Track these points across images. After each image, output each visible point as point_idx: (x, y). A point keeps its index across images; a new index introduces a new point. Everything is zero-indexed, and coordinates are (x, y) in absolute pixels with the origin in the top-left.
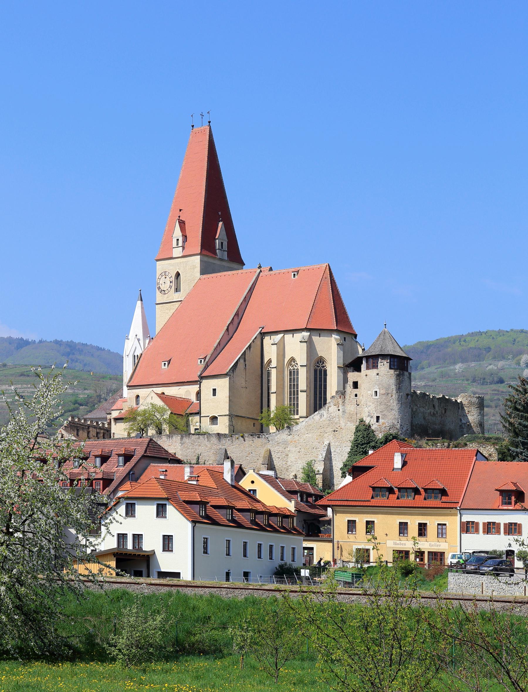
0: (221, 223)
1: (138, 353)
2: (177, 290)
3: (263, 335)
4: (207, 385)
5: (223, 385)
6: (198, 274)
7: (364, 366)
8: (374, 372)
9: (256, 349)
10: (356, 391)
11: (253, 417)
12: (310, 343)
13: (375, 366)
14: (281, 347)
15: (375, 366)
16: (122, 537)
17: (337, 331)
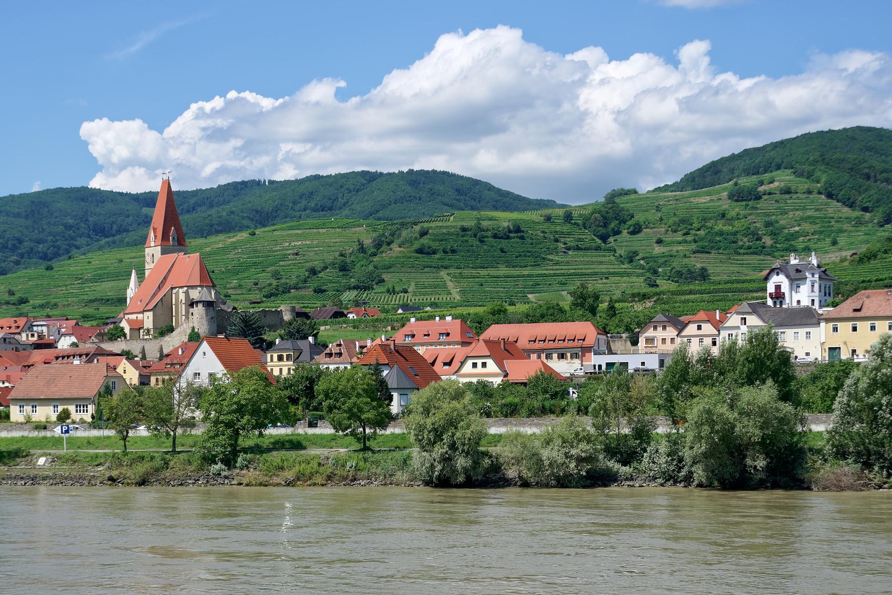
3: (172, 288)
5: (150, 314)
12: (187, 293)
14: (177, 294)
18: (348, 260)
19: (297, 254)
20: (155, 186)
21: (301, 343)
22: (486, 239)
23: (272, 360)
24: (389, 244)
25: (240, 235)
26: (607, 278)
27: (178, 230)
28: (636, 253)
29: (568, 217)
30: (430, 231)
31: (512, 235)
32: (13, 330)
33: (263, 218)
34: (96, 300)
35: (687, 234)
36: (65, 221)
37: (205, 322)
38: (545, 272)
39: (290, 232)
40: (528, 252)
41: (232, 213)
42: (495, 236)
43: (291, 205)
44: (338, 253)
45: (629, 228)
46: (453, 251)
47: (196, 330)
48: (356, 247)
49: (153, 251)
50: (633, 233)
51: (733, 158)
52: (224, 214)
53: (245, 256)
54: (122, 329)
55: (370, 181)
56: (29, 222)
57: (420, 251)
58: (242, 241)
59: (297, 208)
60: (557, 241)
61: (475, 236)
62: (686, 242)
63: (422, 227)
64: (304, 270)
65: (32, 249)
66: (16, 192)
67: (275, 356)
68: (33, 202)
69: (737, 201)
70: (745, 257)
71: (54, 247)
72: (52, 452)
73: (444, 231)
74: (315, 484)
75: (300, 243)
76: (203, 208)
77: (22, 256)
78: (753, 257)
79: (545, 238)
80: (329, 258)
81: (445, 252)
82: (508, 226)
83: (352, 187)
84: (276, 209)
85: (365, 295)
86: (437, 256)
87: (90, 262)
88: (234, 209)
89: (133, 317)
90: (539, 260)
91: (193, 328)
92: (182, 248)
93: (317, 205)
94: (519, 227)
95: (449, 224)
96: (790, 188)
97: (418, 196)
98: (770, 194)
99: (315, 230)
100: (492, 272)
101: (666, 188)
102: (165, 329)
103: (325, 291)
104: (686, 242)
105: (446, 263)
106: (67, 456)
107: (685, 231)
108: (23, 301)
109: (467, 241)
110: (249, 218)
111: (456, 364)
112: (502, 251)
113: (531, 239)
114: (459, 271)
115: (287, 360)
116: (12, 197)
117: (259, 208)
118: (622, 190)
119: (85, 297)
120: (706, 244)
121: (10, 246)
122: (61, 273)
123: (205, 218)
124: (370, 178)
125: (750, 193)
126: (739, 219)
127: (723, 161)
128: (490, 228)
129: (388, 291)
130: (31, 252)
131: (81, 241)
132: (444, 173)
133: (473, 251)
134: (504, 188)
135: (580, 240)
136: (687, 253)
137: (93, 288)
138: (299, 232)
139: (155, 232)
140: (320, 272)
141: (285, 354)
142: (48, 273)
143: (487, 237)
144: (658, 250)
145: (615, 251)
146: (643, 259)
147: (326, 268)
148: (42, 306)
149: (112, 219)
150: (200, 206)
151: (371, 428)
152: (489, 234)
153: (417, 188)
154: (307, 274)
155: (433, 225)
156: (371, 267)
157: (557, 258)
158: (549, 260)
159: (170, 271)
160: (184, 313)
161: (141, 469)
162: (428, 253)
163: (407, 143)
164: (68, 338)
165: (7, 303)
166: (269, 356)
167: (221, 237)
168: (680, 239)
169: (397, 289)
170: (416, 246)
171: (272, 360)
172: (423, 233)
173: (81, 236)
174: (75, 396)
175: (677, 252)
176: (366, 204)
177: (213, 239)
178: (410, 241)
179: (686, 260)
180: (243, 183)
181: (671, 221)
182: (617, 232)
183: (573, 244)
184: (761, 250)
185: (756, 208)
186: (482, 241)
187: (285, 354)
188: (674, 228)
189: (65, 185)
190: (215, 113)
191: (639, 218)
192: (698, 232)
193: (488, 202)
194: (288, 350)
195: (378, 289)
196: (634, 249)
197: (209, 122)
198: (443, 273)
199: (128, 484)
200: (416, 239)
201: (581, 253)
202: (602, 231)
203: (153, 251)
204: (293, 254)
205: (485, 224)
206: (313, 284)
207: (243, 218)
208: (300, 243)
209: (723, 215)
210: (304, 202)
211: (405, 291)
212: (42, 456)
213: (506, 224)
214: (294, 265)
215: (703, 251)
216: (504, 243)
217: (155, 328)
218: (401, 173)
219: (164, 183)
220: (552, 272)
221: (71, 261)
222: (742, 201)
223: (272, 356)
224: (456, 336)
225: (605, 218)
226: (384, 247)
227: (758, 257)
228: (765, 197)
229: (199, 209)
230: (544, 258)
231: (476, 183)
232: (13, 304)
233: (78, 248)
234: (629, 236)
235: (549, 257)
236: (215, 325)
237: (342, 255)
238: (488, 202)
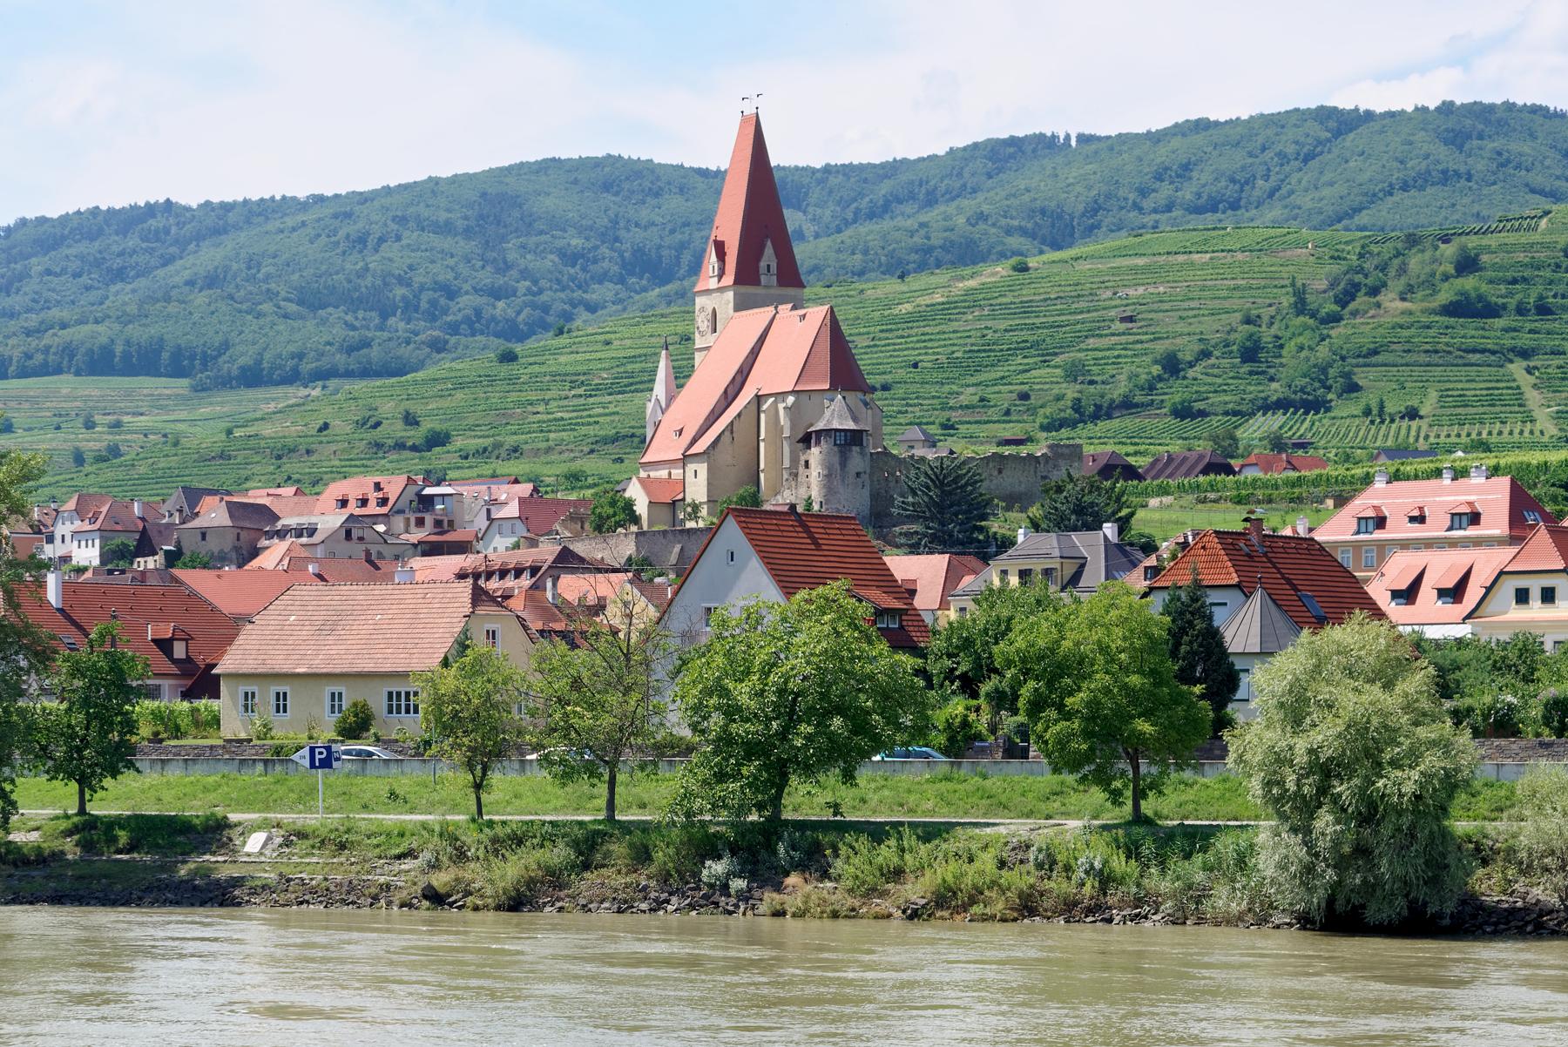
5: (702, 469)
18: (1267, 335)
19: (1130, 319)
21: (1082, 541)
24: (1374, 291)
32: (373, 508)
33: (1058, 230)
34: (615, 439)
36: (560, 243)
41: (982, 217)
44: (1238, 316)
48: (1287, 301)
52: (961, 220)
54: (629, 505)
55: (1338, 134)
56: (472, 246)
57: (1460, 309)
58: (994, 285)
59: (1147, 204)
63: (1463, 249)
64: (1148, 359)
65: (478, 312)
66: (445, 173)
68: (484, 195)
71: (534, 306)
72: (287, 817)
73: (1521, 257)
74: (985, 918)
76: (908, 208)
77: (454, 329)
80: (1211, 328)
83: (1291, 149)
84: (1095, 209)
85: (1307, 424)
86: (1499, 323)
87: (608, 343)
88: (985, 208)
92: (791, 291)
93: (1199, 195)
95: (1535, 237)
97: (1463, 169)
99: (1181, 258)
103: (1203, 414)
105: (1525, 340)
106: (323, 832)
108: (437, 440)
110: (1023, 232)
111: (1473, 594)
116: (434, 182)
119: (591, 430)
121: (424, 305)
122: (536, 369)
124: (1339, 124)
129: (1367, 412)
130: (475, 323)
131: (597, 293)
132: (1536, 110)
137: (612, 409)
140: (1191, 365)
142: (504, 370)
147: (1206, 354)
148: (483, 452)
149: (678, 237)
151: (1152, 762)
153: (1461, 148)
154: (1156, 370)
155: (1492, 241)
156: (1323, 352)
161: (512, 870)
165: (400, 446)
167: (941, 277)
169: (1390, 408)
170: (1445, 295)
173: (601, 279)
174: (387, 668)
176: (1326, 192)
177: (916, 282)
178: (1430, 283)
180: (1013, 141)
189: (565, 153)
195: (1346, 409)
198: (1517, 368)
199: (476, 909)
200: (1446, 278)
204: (1123, 320)
206: (1175, 393)
210: (1165, 191)
211: (1413, 414)
212: (259, 828)
217: (711, 501)
218: (1423, 110)
219: (745, 119)
221: (563, 340)
224: (1496, 523)
226: (1361, 301)
232: (414, 448)
233: (592, 308)
236: (866, 493)
237: (1248, 321)
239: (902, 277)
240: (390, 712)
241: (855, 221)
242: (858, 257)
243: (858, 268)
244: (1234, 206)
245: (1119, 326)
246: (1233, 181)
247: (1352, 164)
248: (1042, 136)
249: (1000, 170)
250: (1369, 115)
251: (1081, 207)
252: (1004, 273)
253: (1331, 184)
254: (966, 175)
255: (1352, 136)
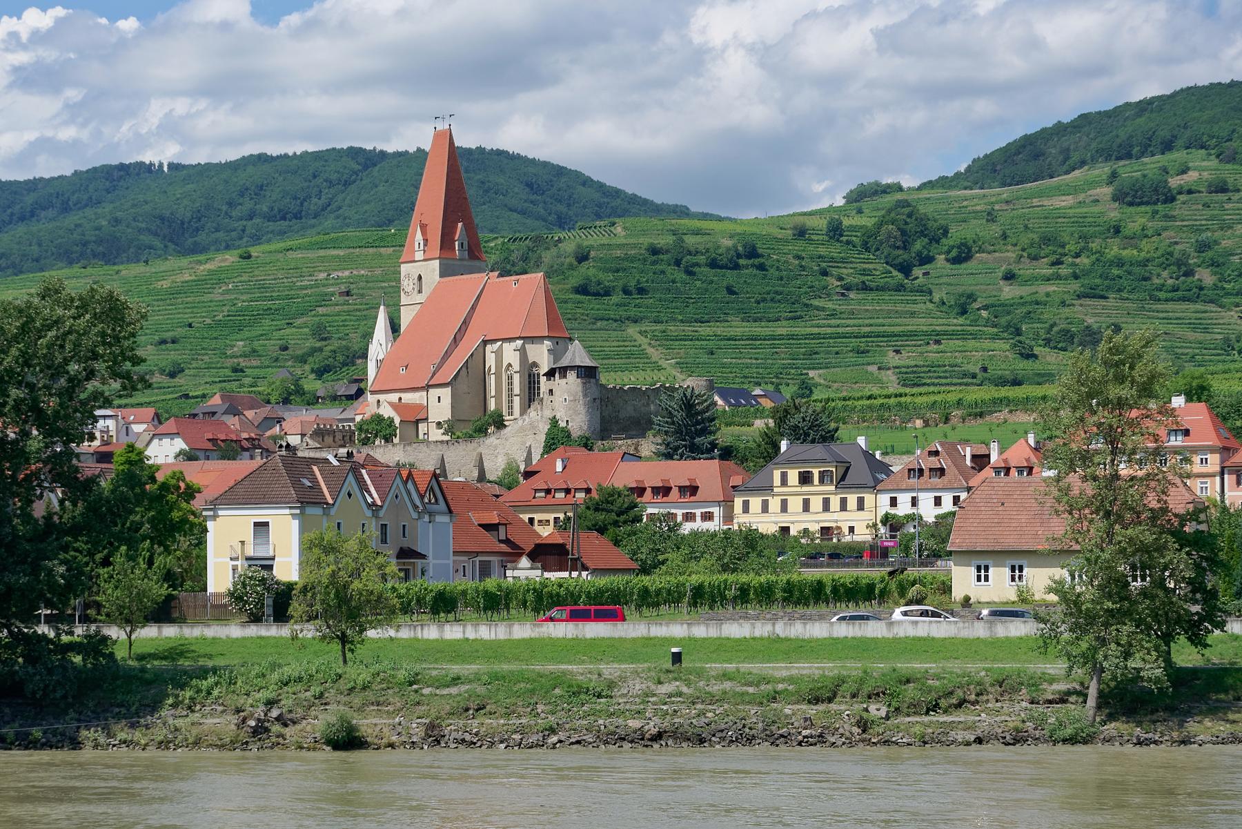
0: (460, 225)
1: (381, 357)
2: (420, 292)
3: (485, 343)
4: (434, 393)
5: (446, 393)
6: (437, 278)
7: (557, 375)
8: (564, 381)
9: (478, 358)
10: (551, 398)
11: (476, 421)
12: (523, 352)
13: (565, 377)
14: (499, 354)
15: (565, 377)
16: (861, 505)
17: (548, 338)
19: (348, 293)
20: (413, 137)
22: (696, 269)
23: (784, 482)
25: (219, 257)
26: (938, 342)
27: (470, 229)
28: (972, 297)
29: (801, 233)
30: (592, 254)
31: (742, 262)
35: (1058, 263)
37: (581, 408)
38: (816, 330)
39: (322, 253)
40: (777, 293)
41: (117, 221)
42: (713, 264)
43: (224, 208)
45: (948, 252)
46: (641, 291)
47: (562, 424)
49: (420, 271)
50: (957, 260)
51: (1060, 130)
53: (244, 298)
55: (366, 167)
57: (582, 290)
60: (825, 273)
61: (678, 263)
62: (1059, 277)
67: (793, 476)
69: (1131, 204)
70: (1170, 306)
73: (618, 253)
75: (347, 273)
76: (51, 213)
78: (1185, 306)
79: (803, 268)
81: (626, 291)
82: (735, 247)
83: (334, 177)
84: (198, 216)
86: (615, 299)
89: (408, 397)
90: (799, 310)
91: (554, 421)
92: (477, 263)
93: (272, 209)
94: (754, 248)
96: (1225, 182)
98: (1190, 192)
99: (371, 250)
100: (720, 329)
101: (943, 183)
102: (476, 421)
104: (1059, 277)
105: (633, 312)
107: (1053, 258)
109: (663, 272)
112: (730, 291)
113: (778, 269)
114: (659, 327)
115: (822, 481)
117: (167, 213)
118: (877, 184)
120: (1098, 281)
123: (71, 231)
125: (1156, 190)
126: (1146, 236)
127: (1045, 135)
128: (701, 248)
133: (678, 291)
134: (611, 181)
135: (865, 272)
136: (1066, 297)
138: (341, 252)
139: (424, 233)
141: (816, 472)
143: (698, 265)
144: (1009, 292)
145: (930, 293)
146: (986, 307)
150: (44, 208)
152: (702, 259)
157: (830, 305)
158: (817, 308)
159: (473, 308)
160: (493, 393)
162: (597, 294)
163: (386, 101)
164: (166, 441)
166: (777, 475)
168: (1049, 271)
171: (784, 482)
172: (582, 257)
175: (1048, 295)
176: (366, 207)
179: (1067, 310)
180: (122, 167)
181: (1025, 240)
182: (927, 260)
183: (857, 280)
184: (1196, 294)
185: (1173, 218)
186: (690, 273)
187: (816, 472)
188: (1033, 251)
190: (38, 38)
191: (958, 233)
192: (1078, 260)
193: (584, 207)
194: (823, 461)
196: (969, 289)
197: (22, 58)
198: (632, 330)
200: (571, 267)
201: (872, 295)
202: (903, 256)
203: (420, 271)
204: (341, 294)
205: (690, 241)
207: (140, 230)
208: (347, 273)
209: (1117, 230)
210: (248, 205)
213: (728, 243)
214: (348, 313)
215: (1092, 294)
216: (730, 277)
220: (829, 330)
222: (1141, 204)
223: (784, 477)
225: (903, 233)
227: (1192, 307)
228: (1182, 198)
229: (43, 214)
230: (806, 305)
231: (560, 171)
234: (948, 265)
235: (816, 302)
238: (584, 207)
239: (146, 262)
240: (979, 579)
241: (10, 223)
242: (35, 248)
243: (35, 256)
244: (297, 216)
245: (342, 299)
246: (295, 198)
247: (381, 188)
248: (142, 163)
249: (115, 188)
250: (383, 154)
251: (189, 215)
252: (232, 259)
253: (368, 203)
254: (91, 189)
255: (377, 168)
